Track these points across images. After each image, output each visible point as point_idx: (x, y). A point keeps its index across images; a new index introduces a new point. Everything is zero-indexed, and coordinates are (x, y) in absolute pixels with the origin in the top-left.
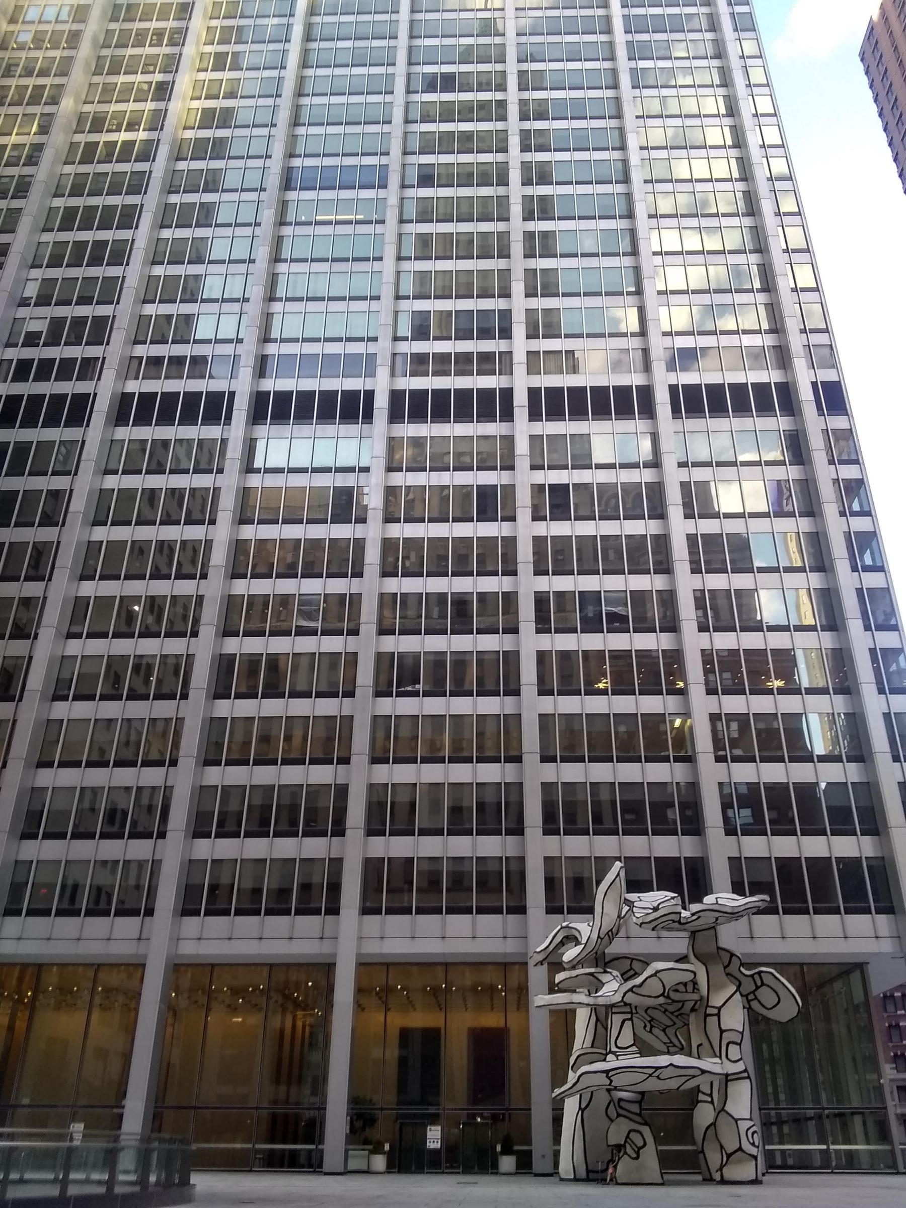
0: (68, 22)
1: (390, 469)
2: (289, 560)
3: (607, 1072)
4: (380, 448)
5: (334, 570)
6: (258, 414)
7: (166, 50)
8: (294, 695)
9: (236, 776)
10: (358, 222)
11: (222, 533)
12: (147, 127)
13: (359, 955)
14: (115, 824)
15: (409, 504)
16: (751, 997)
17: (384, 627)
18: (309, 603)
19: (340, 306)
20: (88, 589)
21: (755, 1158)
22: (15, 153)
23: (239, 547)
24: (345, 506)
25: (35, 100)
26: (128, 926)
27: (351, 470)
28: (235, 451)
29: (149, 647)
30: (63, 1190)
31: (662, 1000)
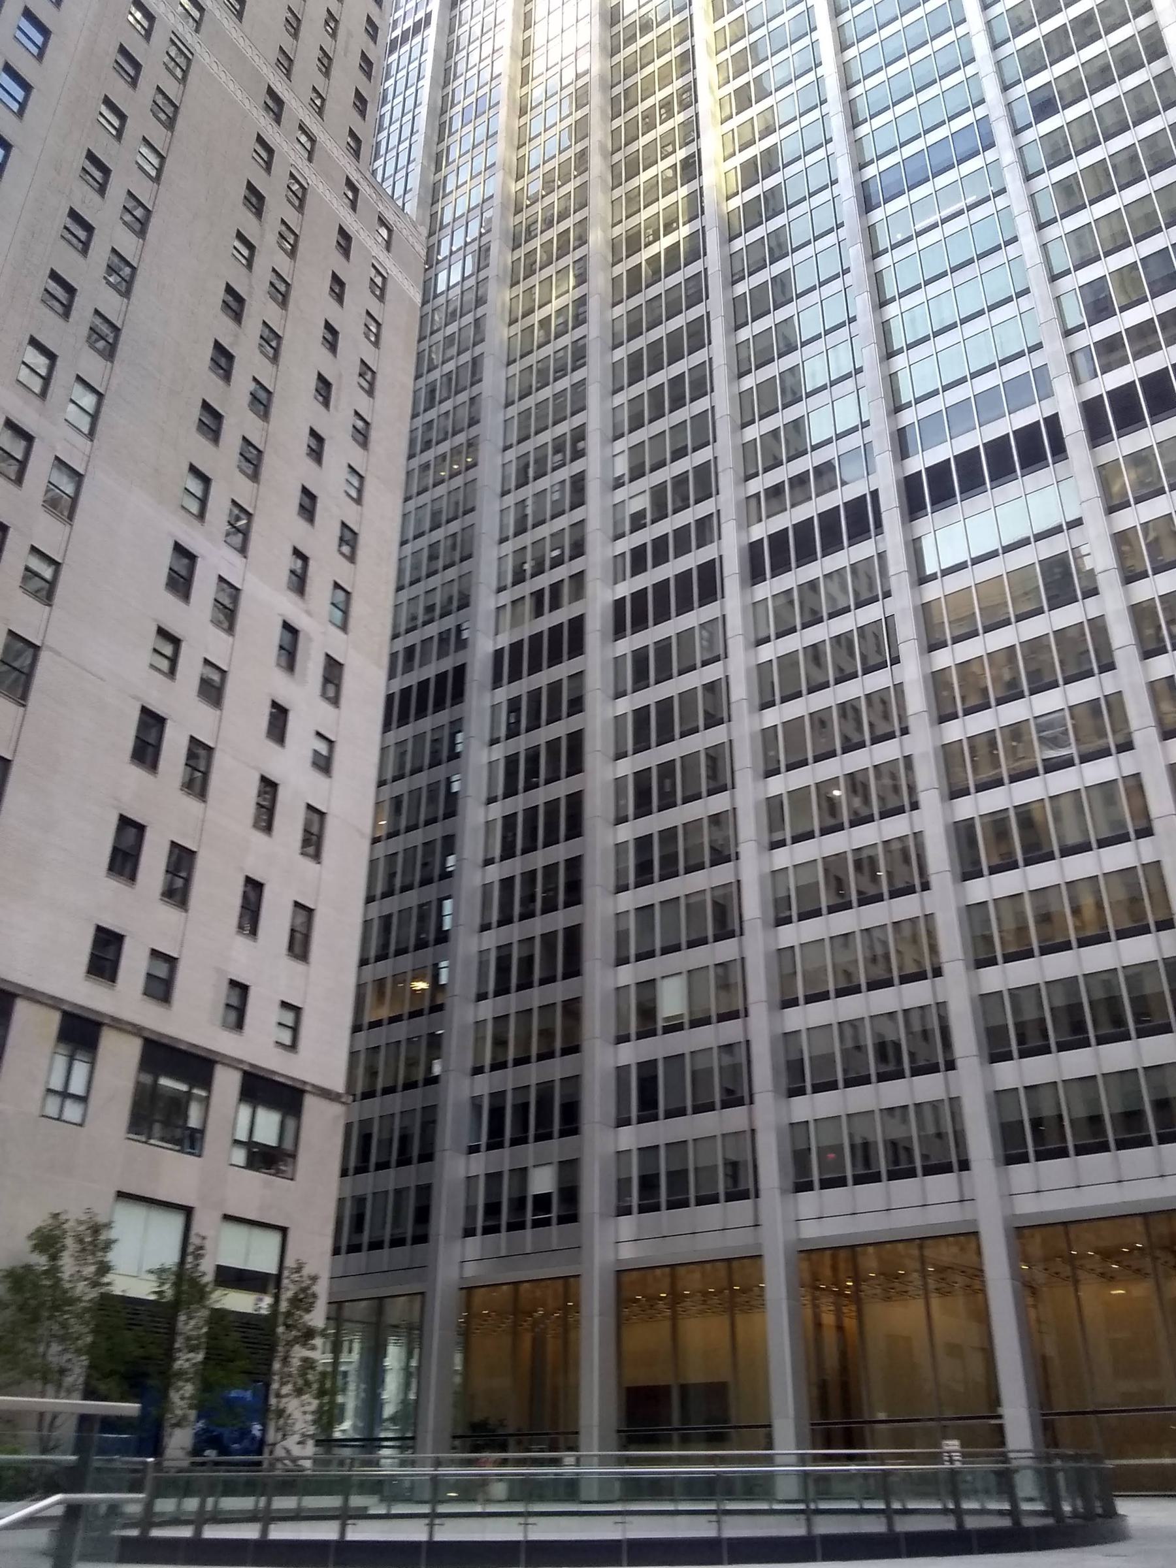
0: (570, 146)
1: (1111, 510)
2: (1007, 676)
4: (1089, 486)
5: (1073, 671)
6: (913, 507)
7: (680, 118)
8: (1067, 852)
9: (1022, 973)
10: (970, 208)
11: (911, 671)
12: (686, 219)
14: (890, 1062)
15: (1154, 546)
17: (1168, 728)
18: (1049, 726)
19: (980, 324)
20: (777, 786)
22: (561, 320)
23: (937, 681)
24: (1062, 581)
25: (563, 251)
26: (942, 1185)
27: (1057, 530)
28: (898, 563)
29: (866, 836)
30: (960, 1523)
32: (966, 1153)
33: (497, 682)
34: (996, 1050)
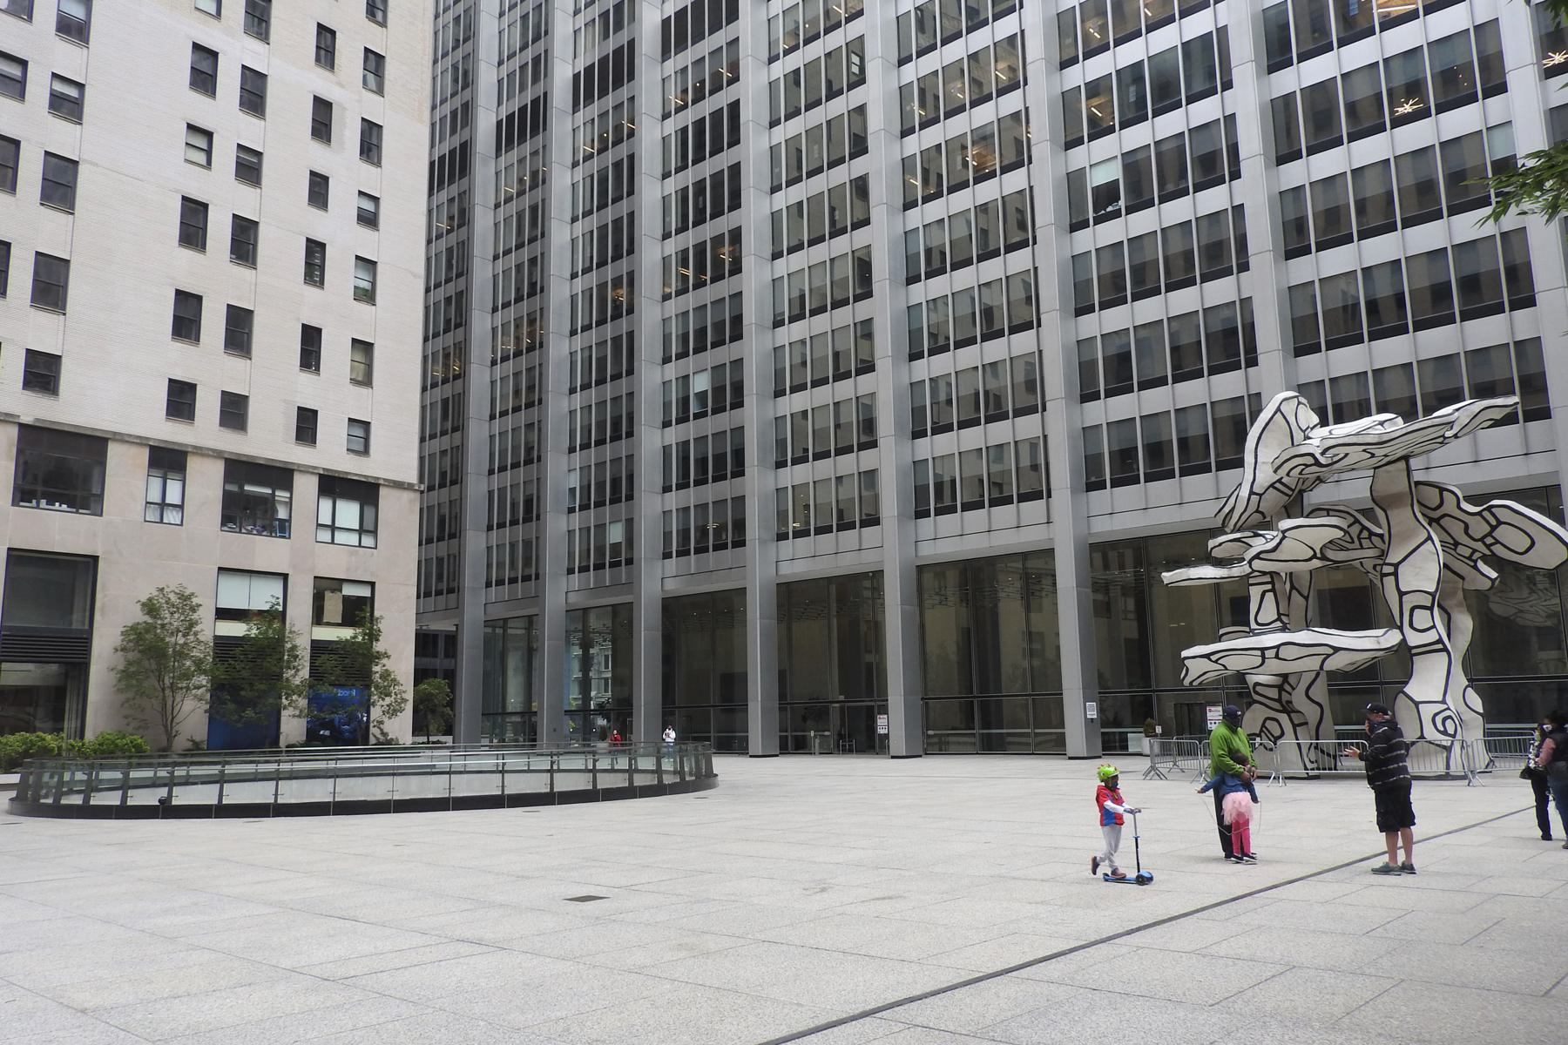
26: (1034, 509)
31: (1316, 563)
33: (665, 54)
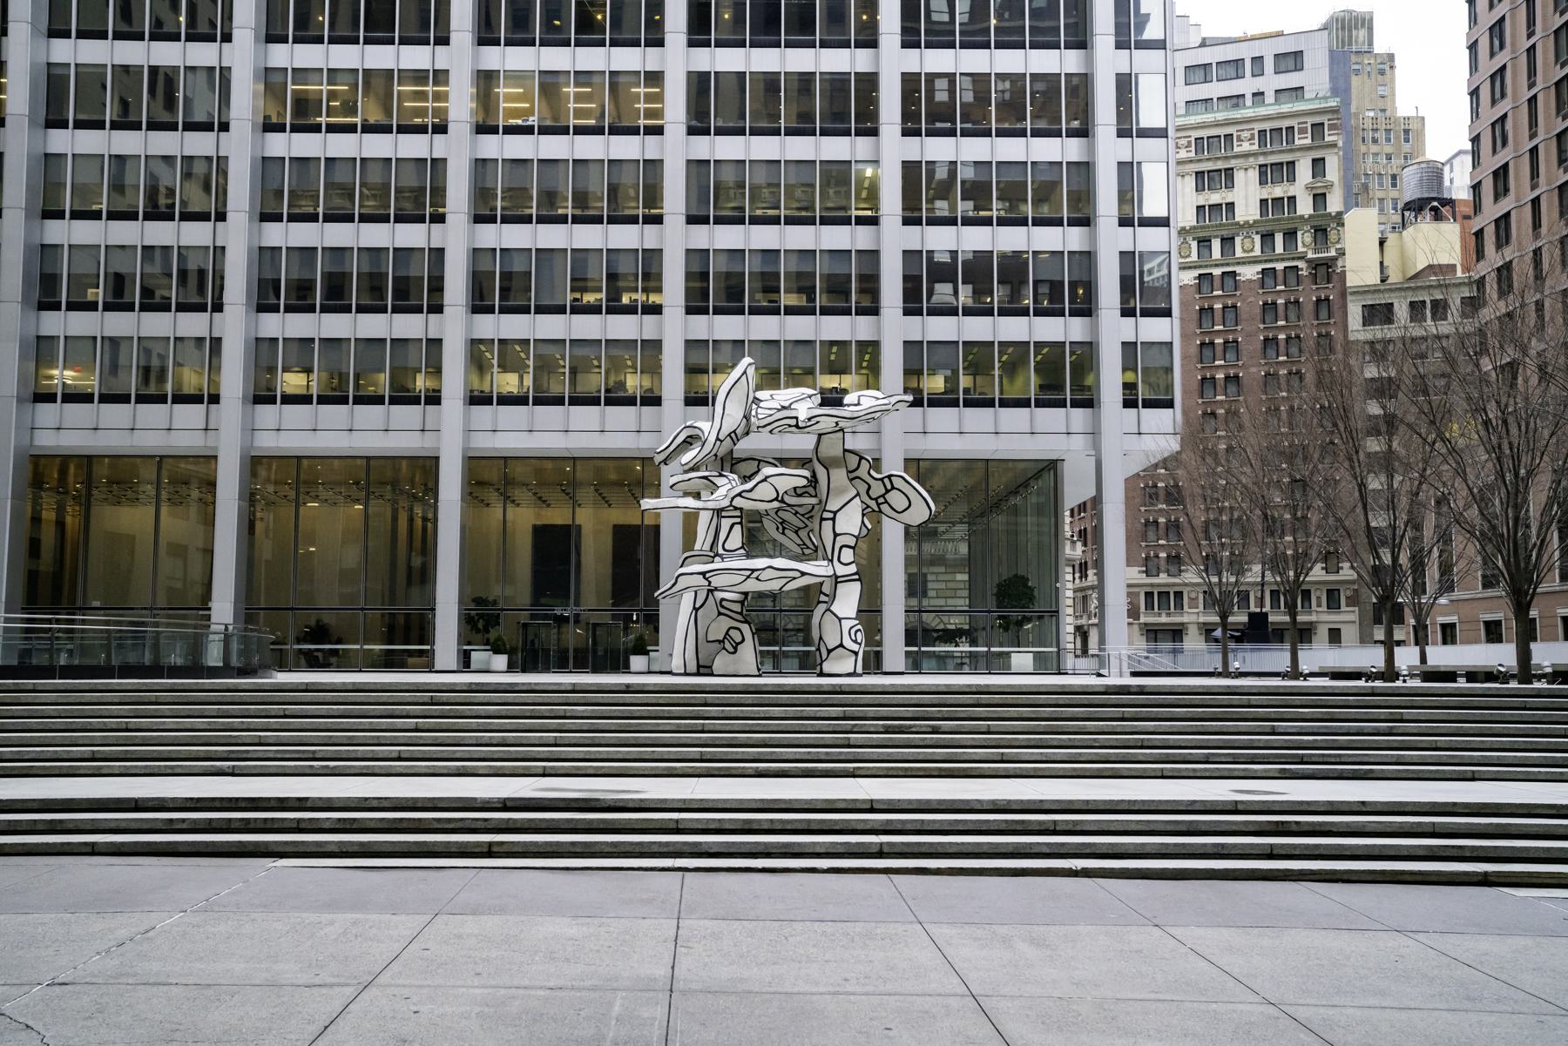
3: (703, 574)
13: (465, 450)
16: (881, 500)
21: (856, 653)
31: (776, 504)
32: (225, 205)
34: (265, 299)
